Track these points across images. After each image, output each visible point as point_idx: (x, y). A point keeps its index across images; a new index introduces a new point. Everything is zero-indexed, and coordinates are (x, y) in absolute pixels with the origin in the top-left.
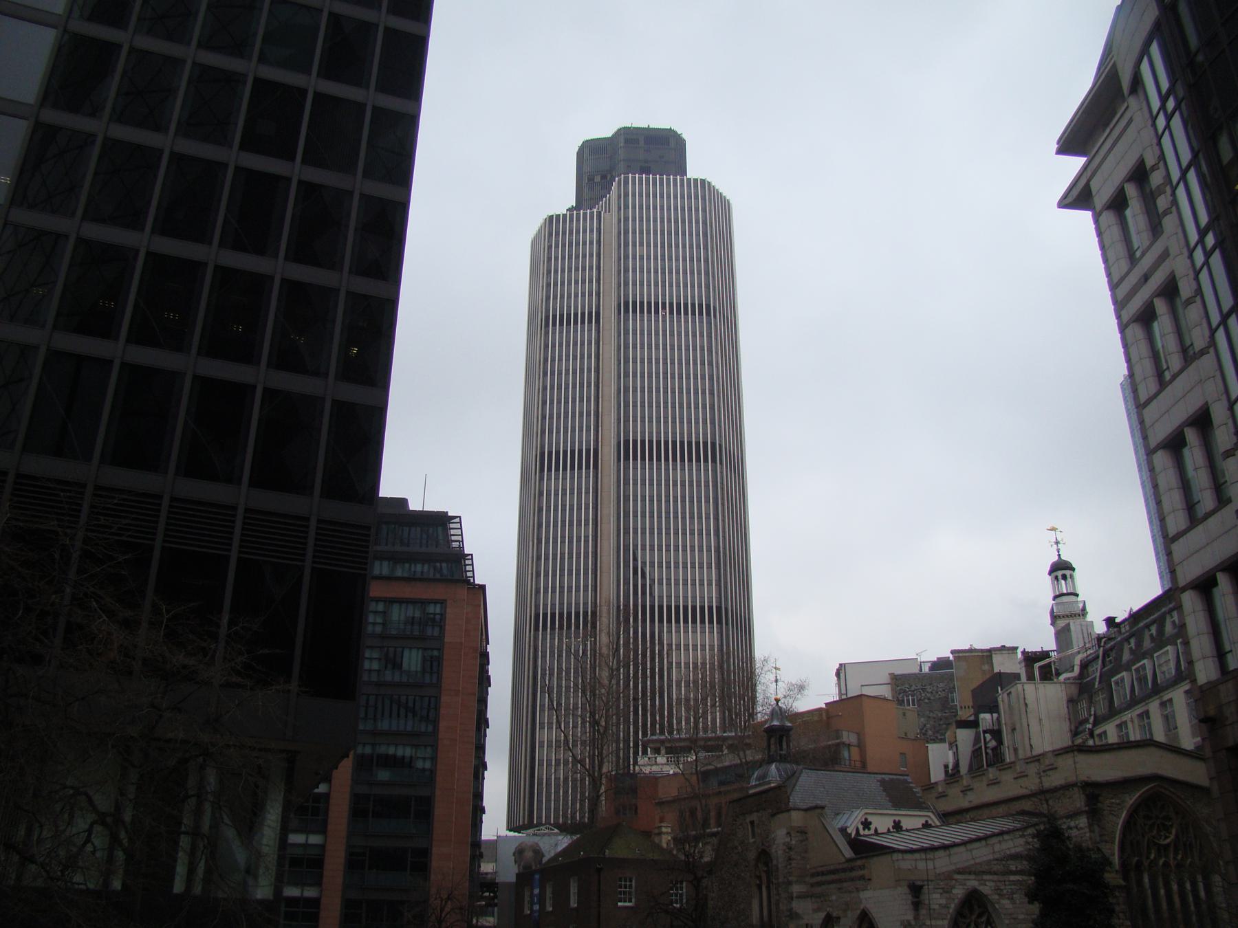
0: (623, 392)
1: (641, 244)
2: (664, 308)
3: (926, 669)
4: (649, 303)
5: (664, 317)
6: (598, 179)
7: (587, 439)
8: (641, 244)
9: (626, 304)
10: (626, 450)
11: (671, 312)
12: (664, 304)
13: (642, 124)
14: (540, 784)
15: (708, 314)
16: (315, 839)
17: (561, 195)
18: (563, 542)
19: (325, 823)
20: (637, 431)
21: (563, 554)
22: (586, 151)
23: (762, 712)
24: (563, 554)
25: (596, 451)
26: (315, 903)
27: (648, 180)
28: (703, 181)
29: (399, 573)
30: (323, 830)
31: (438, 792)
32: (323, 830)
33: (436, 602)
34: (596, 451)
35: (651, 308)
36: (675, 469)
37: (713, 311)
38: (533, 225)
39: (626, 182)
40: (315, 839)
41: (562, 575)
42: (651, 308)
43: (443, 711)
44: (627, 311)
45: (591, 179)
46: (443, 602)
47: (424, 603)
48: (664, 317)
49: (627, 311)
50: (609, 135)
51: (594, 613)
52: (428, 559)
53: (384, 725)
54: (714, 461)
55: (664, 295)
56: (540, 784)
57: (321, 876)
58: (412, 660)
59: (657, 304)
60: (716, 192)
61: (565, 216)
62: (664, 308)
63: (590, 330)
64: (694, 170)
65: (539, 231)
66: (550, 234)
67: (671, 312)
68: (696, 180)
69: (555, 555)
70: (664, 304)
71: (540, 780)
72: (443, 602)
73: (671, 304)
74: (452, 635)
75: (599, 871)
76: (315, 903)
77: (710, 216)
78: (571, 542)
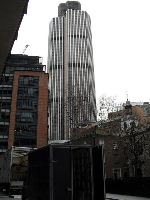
0: (69, 53)
1: (72, 24)
2: (77, 36)
3: (143, 104)
4: (74, 35)
5: (77, 38)
6: (63, 11)
7: (61, 63)
8: (72, 24)
9: (69, 35)
10: (70, 65)
11: (79, 37)
12: (77, 36)
13: (36, 56)
14: (52, 134)
15: (87, 38)
16: (5, 137)
17: (55, 14)
18: (56, 84)
19: (8, 133)
20: (72, 61)
21: (56, 86)
22: (60, 6)
23: (102, 116)
24: (56, 86)
25: (63, 65)
26: (8, 126)
27: (74, 11)
28: (85, 11)
29: (27, 70)
30: (8, 134)
31: (38, 124)
32: (8, 134)
33: (36, 77)
34: (63, 65)
35: (75, 36)
36: (80, 69)
37: (86, 37)
38: (50, 20)
39: (69, 11)
40: (5, 137)
41: (56, 91)
42: (75, 36)
43: (39, 104)
44: (70, 37)
45: (61, 11)
46: (38, 77)
47: (33, 77)
48: (77, 38)
49: (70, 37)
50: (65, 2)
51: (63, 99)
52: (35, 67)
53: (23, 107)
54: (88, 67)
55: (77, 34)
56: (52, 134)
57: (10, 108)
58: (31, 91)
59: (76, 36)
60: (88, 14)
61: (58, 18)
62: (77, 36)
63: (62, 41)
64: (83, 9)
65: (51, 22)
66: (53, 22)
67: (79, 37)
68: (84, 11)
69: (55, 87)
70: (77, 36)
71: (52, 133)
72: (38, 77)
73: (79, 36)
74: (41, 84)
75: (94, 138)
76: (8, 126)
77: (86, 18)
78: (58, 84)
